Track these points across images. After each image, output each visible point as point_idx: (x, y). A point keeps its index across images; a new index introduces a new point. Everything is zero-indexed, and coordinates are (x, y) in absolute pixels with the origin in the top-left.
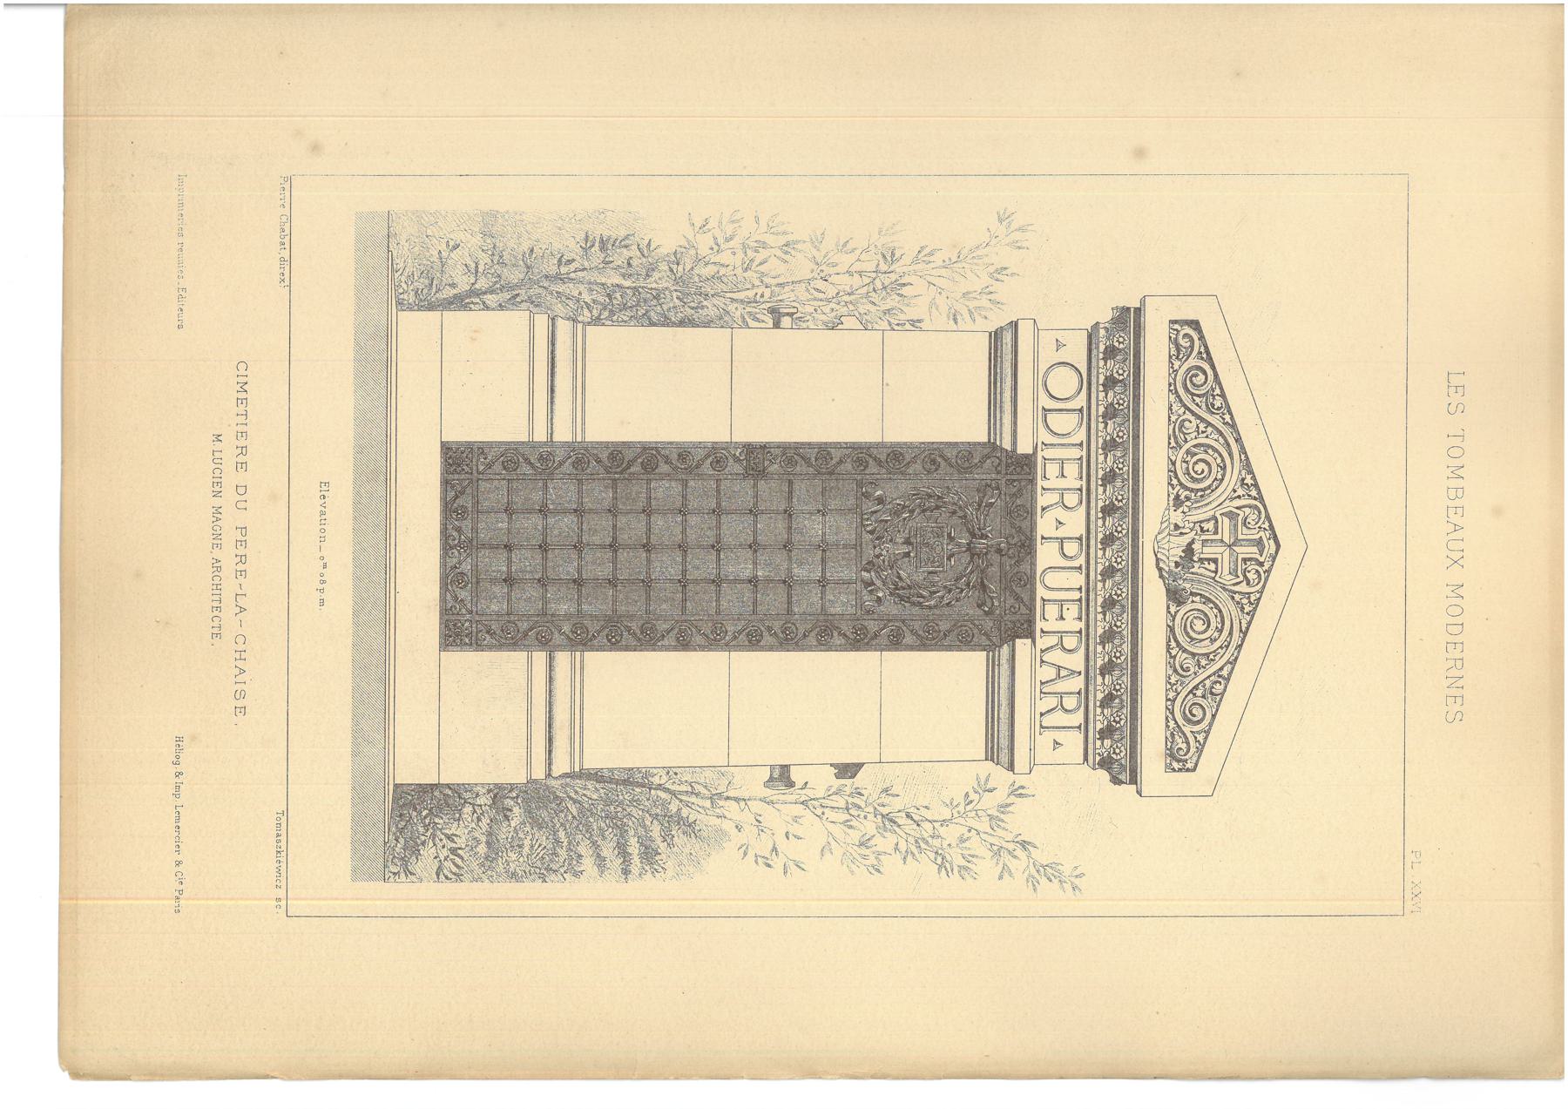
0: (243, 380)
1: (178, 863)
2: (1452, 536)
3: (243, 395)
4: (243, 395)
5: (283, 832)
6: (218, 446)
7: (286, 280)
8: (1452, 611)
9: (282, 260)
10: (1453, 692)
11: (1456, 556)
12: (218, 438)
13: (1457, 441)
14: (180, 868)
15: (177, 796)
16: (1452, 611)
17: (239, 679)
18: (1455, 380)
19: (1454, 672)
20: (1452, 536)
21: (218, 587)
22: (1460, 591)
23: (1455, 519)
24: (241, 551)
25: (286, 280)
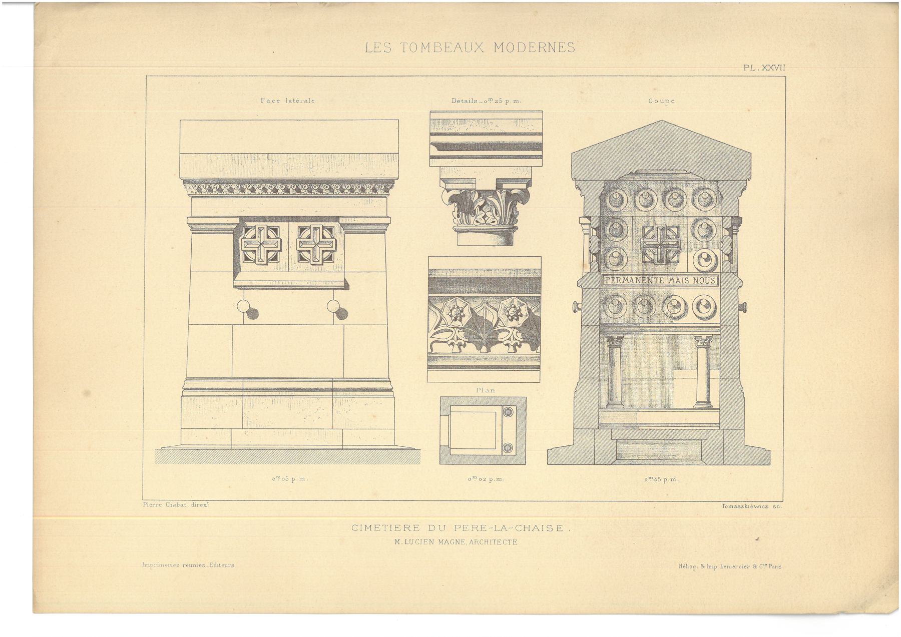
0: (363, 527)
1: (755, 566)
2: (463, 49)
3: (373, 527)
4: (373, 527)
5: (734, 504)
6: (402, 541)
7: (205, 503)
8: (414, 49)
9: (193, 505)
10: (432, 48)
11: (475, 47)
12: (397, 541)
13: (407, 47)
14: (758, 566)
15: (715, 568)
16: (414, 49)
17: (540, 529)
18: (371, 48)
19: (547, 48)
20: (463, 49)
21: (487, 542)
22: (425, 45)
23: (452, 47)
24: (402, 528)
25: (205, 503)
